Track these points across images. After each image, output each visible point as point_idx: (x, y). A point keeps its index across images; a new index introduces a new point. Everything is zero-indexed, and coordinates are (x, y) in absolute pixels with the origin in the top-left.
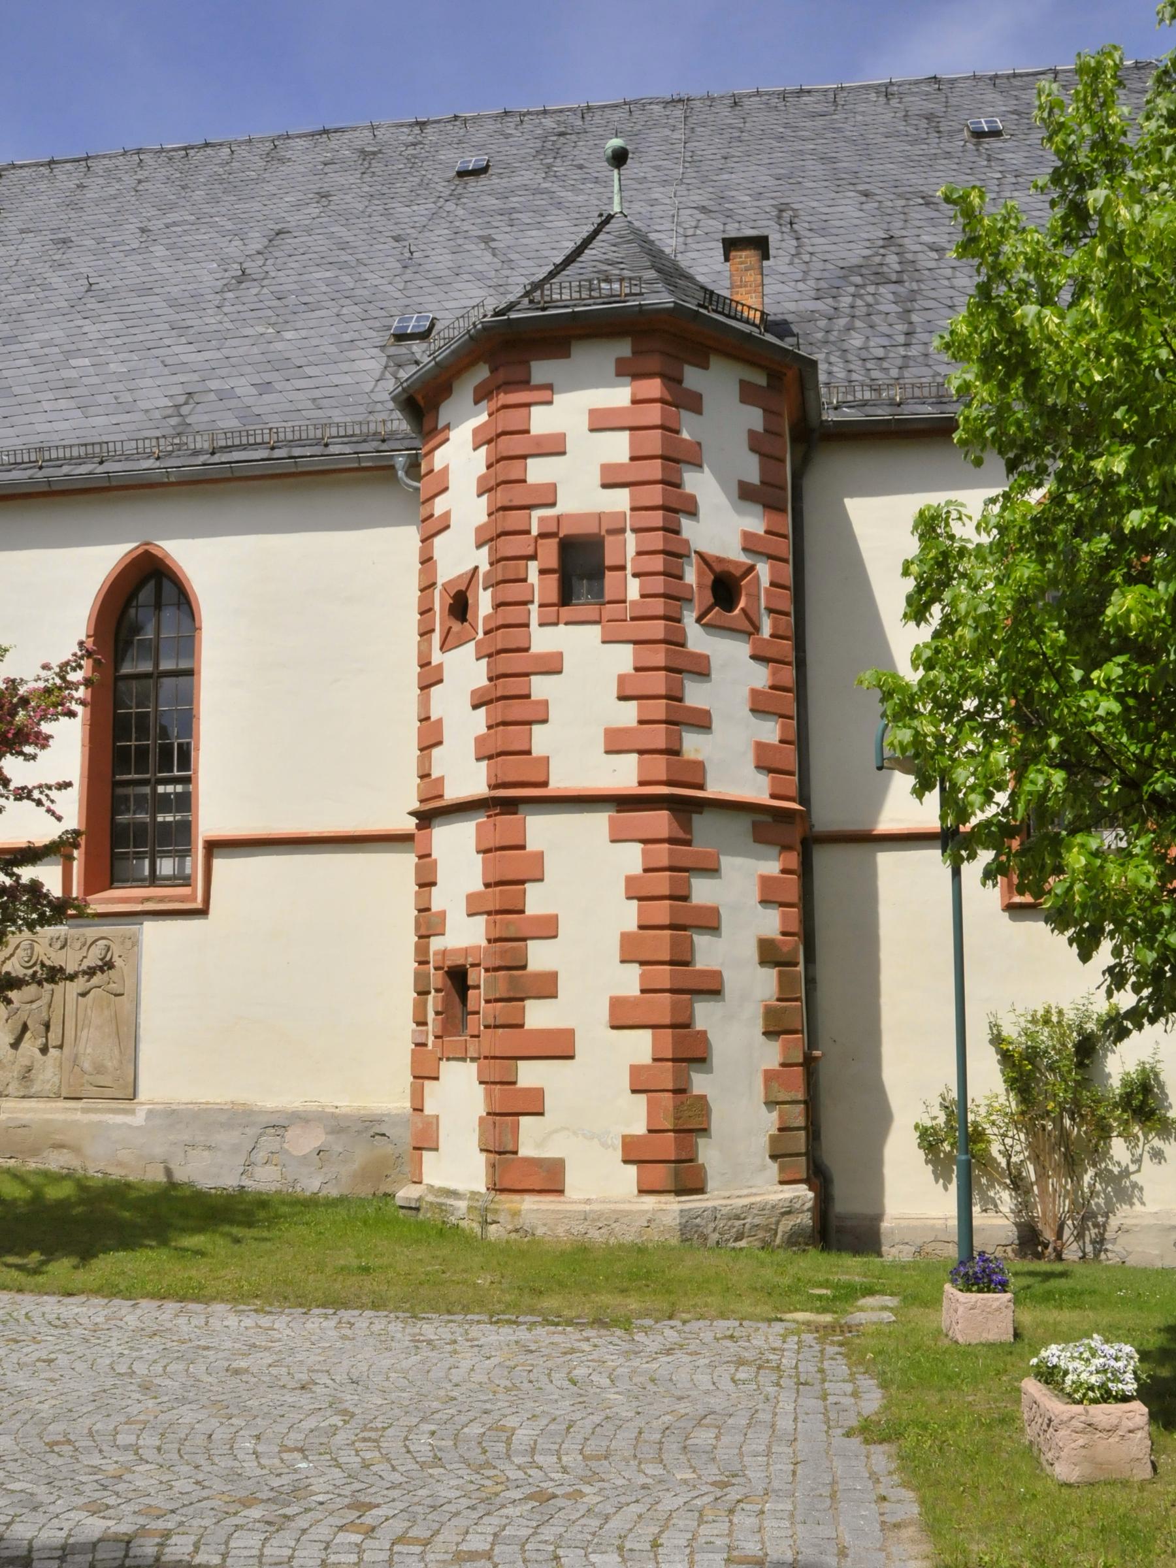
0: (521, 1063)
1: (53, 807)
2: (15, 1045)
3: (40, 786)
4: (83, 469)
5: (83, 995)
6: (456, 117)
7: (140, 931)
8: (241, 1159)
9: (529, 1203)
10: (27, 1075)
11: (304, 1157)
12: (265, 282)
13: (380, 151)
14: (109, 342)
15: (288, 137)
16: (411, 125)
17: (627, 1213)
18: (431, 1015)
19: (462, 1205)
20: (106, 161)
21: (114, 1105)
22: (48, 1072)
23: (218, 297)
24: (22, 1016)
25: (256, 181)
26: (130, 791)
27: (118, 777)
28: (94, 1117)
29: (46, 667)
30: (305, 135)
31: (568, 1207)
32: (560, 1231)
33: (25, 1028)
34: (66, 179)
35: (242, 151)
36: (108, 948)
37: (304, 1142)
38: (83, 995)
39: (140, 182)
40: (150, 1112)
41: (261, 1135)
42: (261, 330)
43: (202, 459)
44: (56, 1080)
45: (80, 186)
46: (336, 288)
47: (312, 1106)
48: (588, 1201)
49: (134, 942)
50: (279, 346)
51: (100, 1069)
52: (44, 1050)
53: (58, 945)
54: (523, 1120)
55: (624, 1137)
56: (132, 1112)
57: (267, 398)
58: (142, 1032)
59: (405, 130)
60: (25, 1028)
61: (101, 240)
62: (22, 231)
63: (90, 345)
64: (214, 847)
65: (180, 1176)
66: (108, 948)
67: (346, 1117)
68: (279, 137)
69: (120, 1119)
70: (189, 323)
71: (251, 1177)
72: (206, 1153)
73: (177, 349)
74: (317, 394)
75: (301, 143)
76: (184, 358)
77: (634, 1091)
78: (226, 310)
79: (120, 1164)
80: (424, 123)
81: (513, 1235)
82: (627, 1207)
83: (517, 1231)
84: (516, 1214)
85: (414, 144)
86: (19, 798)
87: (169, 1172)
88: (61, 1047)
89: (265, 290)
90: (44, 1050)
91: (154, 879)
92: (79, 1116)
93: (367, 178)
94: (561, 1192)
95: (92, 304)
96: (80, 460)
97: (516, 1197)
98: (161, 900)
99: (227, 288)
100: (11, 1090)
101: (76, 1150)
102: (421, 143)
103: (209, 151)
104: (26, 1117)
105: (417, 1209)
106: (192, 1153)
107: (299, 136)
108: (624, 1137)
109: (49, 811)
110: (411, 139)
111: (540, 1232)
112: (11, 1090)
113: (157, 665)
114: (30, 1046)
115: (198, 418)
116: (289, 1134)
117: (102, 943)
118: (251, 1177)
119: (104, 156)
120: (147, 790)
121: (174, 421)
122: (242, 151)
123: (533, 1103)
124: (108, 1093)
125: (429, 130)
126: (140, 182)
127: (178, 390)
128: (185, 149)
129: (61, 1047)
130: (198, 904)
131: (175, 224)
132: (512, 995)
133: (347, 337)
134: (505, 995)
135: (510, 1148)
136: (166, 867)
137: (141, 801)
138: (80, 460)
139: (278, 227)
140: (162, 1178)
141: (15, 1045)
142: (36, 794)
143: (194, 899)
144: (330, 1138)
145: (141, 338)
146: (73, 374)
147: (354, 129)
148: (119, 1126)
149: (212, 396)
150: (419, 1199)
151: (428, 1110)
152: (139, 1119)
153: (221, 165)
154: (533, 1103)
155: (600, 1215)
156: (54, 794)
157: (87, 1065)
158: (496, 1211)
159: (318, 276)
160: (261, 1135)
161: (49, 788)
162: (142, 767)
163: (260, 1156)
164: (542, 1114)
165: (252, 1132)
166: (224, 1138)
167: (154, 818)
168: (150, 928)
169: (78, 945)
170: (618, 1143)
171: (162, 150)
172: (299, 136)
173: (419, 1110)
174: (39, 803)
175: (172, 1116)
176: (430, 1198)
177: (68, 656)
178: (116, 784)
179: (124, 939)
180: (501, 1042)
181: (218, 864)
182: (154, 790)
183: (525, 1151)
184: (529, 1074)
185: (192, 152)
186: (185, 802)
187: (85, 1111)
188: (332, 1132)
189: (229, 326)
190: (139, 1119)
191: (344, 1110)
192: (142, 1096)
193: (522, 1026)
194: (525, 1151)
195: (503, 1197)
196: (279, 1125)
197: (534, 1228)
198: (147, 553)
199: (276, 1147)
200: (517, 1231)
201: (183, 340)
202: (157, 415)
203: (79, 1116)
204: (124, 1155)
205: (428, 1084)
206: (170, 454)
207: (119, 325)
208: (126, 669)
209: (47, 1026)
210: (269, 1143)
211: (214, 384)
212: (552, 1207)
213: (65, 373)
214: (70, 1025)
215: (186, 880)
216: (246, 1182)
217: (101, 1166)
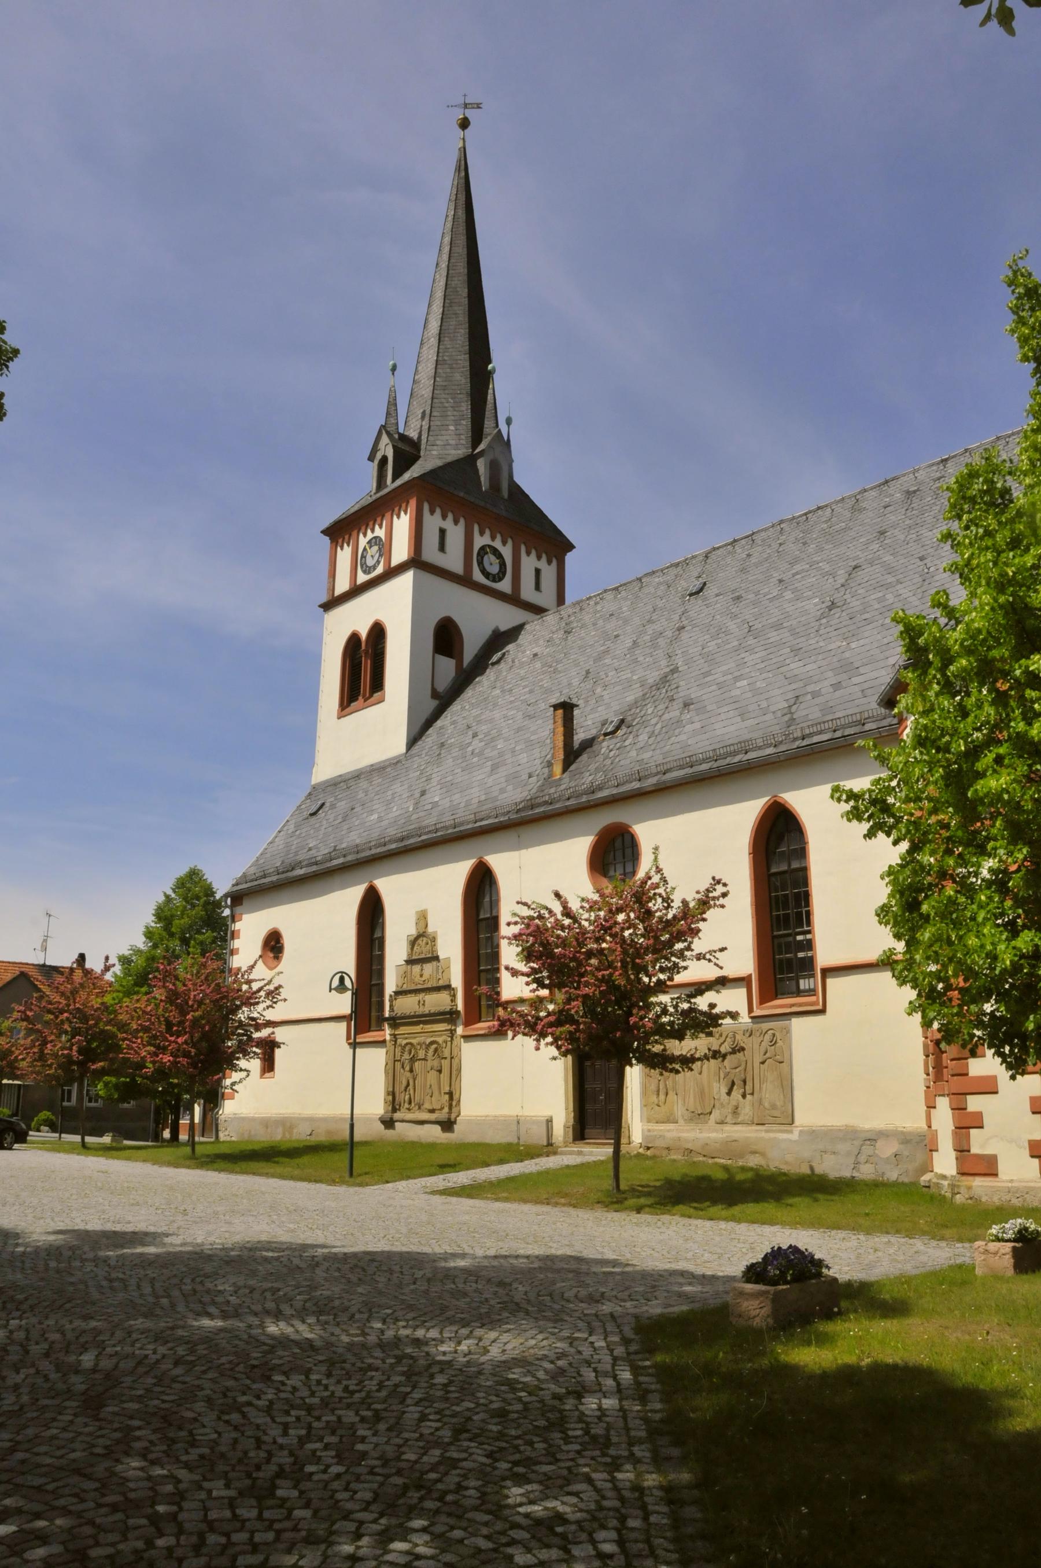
0: (968, 1097)
1: (717, 962)
2: (729, 1093)
3: (710, 952)
4: (737, 759)
5: (763, 1063)
6: (966, 450)
7: (790, 1024)
8: (852, 1160)
9: (978, 1182)
10: (736, 1111)
11: (888, 1158)
12: (844, 607)
13: (918, 490)
14: (758, 667)
15: (865, 491)
16: (938, 464)
17: (1034, 1188)
18: (931, 1069)
19: (946, 1183)
20: (763, 534)
21: (783, 1127)
22: (747, 1108)
23: (818, 623)
24: (731, 1077)
25: (845, 530)
26: (782, 940)
27: (775, 933)
28: (772, 1135)
29: (698, 892)
30: (875, 487)
31: (999, 1184)
32: (996, 1199)
33: (733, 1084)
34: (740, 551)
35: (838, 508)
36: (774, 1035)
37: (887, 1149)
38: (763, 1063)
39: (781, 544)
40: (801, 1131)
41: (862, 1145)
42: (839, 644)
43: (798, 743)
44: (751, 1113)
45: (749, 555)
46: (883, 604)
47: (890, 1127)
48: (1011, 1181)
49: (788, 1031)
50: (847, 655)
51: (774, 1107)
52: (744, 1096)
53: (747, 1034)
54: (972, 1131)
55: (1030, 1142)
56: (791, 1132)
57: (838, 693)
58: (795, 1084)
59: (935, 468)
60: (733, 1084)
61: (757, 594)
62: (717, 595)
63: (748, 670)
64: (827, 972)
65: (819, 1170)
66: (774, 1035)
67: (910, 1133)
68: (860, 493)
69: (784, 1136)
70: (800, 646)
71: (858, 1171)
72: (833, 1156)
73: (792, 666)
74: (866, 685)
75: (873, 493)
76: (796, 672)
77: (1034, 1113)
78: (821, 632)
79: (786, 1163)
80: (946, 460)
81: (969, 1201)
82: (1032, 1184)
83: (971, 1198)
84: (969, 1188)
85: (939, 479)
86: (698, 959)
87: (812, 1168)
88: (752, 1094)
89: (844, 614)
90: (744, 1096)
91: (799, 993)
92: (763, 1134)
93: (909, 513)
94: (996, 1175)
95: (751, 641)
96: (735, 753)
97: (970, 1178)
98: (800, 1005)
99: (823, 616)
100: (728, 1120)
101: (763, 1154)
102: (943, 477)
103: (820, 512)
104: (736, 1136)
105: (929, 1187)
106: (825, 1156)
107: (872, 489)
108: (1030, 1142)
109: (716, 964)
110: (938, 475)
111: (984, 1200)
112: (728, 1120)
113: (789, 865)
114: (736, 1094)
115: (800, 713)
116: (879, 1144)
117: (770, 1032)
118: (858, 1171)
119: (762, 530)
120: (791, 939)
121: (786, 718)
122: (838, 508)
123: (976, 1122)
124: (778, 1120)
125: (949, 464)
126: (781, 544)
127: (790, 695)
128: (806, 514)
129: (752, 1094)
130: (820, 1007)
131: (797, 573)
132: (960, 1056)
133: (886, 641)
134: (957, 1056)
135: (965, 1148)
136: (803, 984)
137: (788, 945)
138: (735, 753)
139: (854, 563)
140: (809, 1172)
141: (729, 1093)
142: (708, 956)
143: (818, 1004)
144: (902, 1146)
145: (774, 661)
146: (738, 692)
147: (904, 475)
148: (785, 1140)
149: (809, 697)
150: (929, 1181)
151: (933, 1128)
152: (795, 1136)
153: (826, 522)
154: (976, 1122)
155: (1018, 1189)
156: (718, 954)
157: (766, 1105)
158: (959, 1186)
159: (873, 597)
160: (862, 1145)
161: (715, 952)
162: (787, 926)
163: (862, 1158)
164: (982, 1127)
165: (857, 1143)
166: (842, 1147)
167: (796, 955)
168: (796, 1022)
169: (758, 1034)
170: (1027, 1145)
171: (794, 518)
172: (872, 489)
173: (930, 1127)
174: (710, 960)
175: (813, 1134)
176: (935, 1180)
177: (707, 886)
178: (774, 937)
179: (782, 1029)
180: (956, 1084)
181: (830, 982)
182: (795, 939)
183: (975, 1150)
184: (974, 1103)
185: (810, 515)
186: (809, 945)
187: (767, 1131)
188: (902, 1143)
189: (822, 644)
190: (795, 1136)
191: (909, 1129)
192: (797, 1122)
193: (967, 1074)
194: (975, 1150)
195: (964, 1178)
196: (872, 1138)
197: (980, 1197)
198: (775, 802)
199: (871, 1153)
200: (971, 1198)
201: (797, 658)
202: (779, 714)
203: (763, 1134)
204: (789, 1158)
205: (932, 1110)
206: (781, 742)
207: (764, 653)
208: (774, 870)
209: (745, 1082)
210: (867, 1150)
211: (810, 689)
212: (990, 1184)
213: (733, 693)
214: (757, 1081)
215: (812, 992)
216: (855, 1174)
217: (777, 1164)
